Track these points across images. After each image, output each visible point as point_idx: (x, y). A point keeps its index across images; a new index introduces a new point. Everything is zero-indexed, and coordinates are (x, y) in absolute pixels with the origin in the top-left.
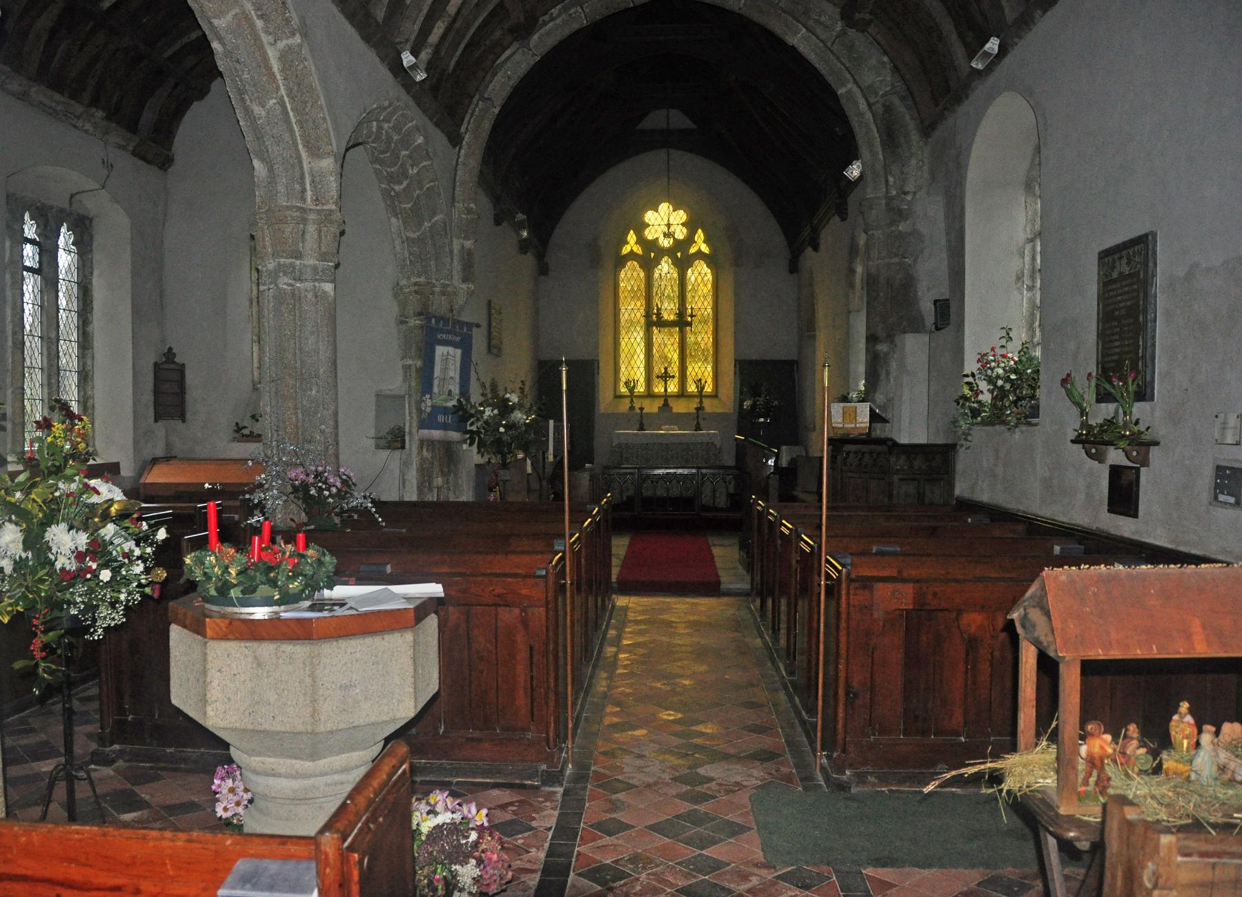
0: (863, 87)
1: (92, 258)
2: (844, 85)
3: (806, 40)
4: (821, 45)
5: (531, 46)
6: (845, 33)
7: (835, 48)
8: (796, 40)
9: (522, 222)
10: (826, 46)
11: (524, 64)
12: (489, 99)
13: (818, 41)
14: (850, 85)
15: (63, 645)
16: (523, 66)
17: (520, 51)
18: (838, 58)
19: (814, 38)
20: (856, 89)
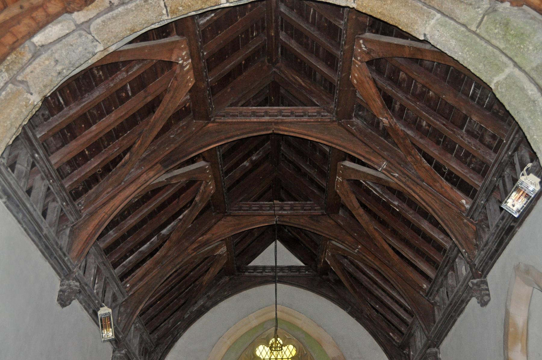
0: (527, 69)
1: (88, 312)
2: (500, 70)
3: (442, 25)
4: (463, 29)
5: (92, 29)
6: (495, 11)
7: (481, 31)
8: (428, 29)
9: (107, 317)
10: (470, 31)
11: (80, 49)
12: (22, 82)
13: (458, 26)
14: (510, 69)
15: (357, 71)
16: (78, 51)
17: (76, 33)
18: (488, 42)
19: (453, 22)
20: (517, 71)
